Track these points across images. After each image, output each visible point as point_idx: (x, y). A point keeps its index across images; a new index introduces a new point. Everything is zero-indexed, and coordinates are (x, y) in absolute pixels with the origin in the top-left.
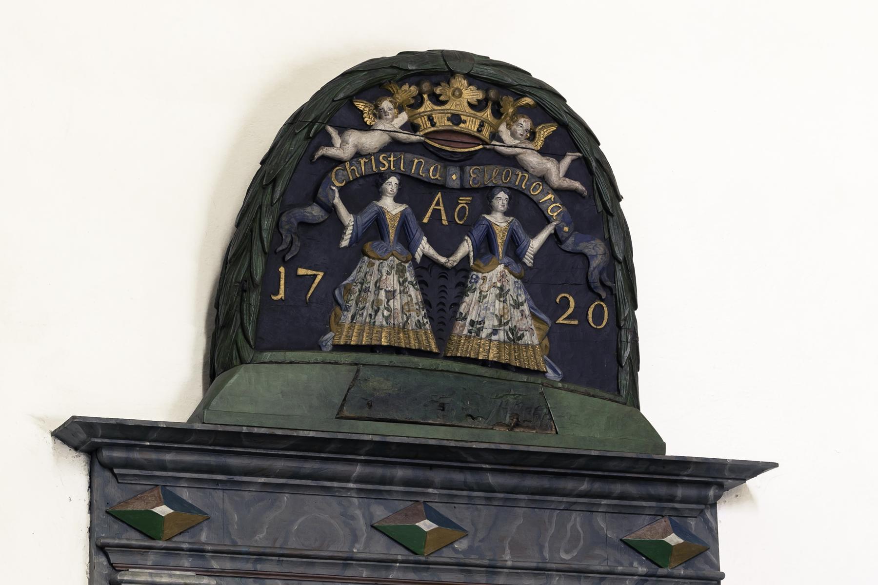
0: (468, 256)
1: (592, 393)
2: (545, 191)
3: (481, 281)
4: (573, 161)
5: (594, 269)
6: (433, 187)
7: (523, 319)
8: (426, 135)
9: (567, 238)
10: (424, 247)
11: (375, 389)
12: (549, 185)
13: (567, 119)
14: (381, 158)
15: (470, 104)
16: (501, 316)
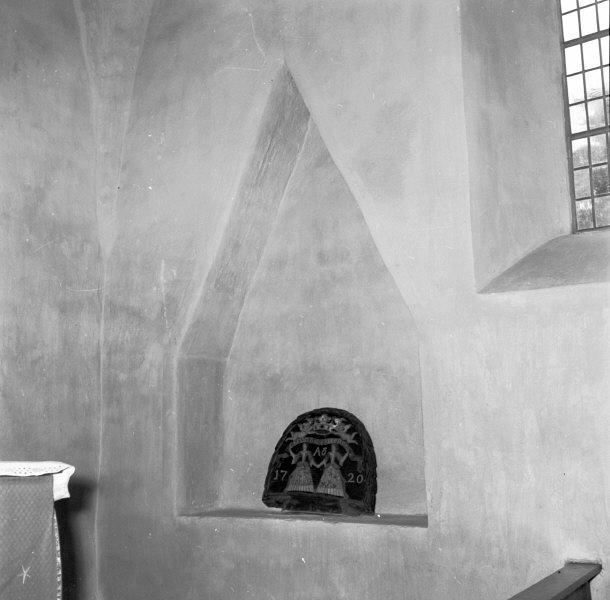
10: (313, 463)
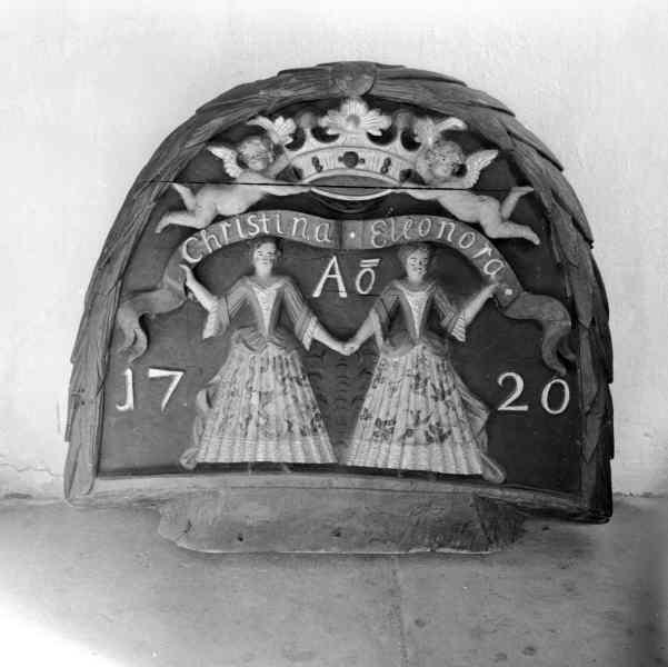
10: (312, 332)
15: (373, 138)
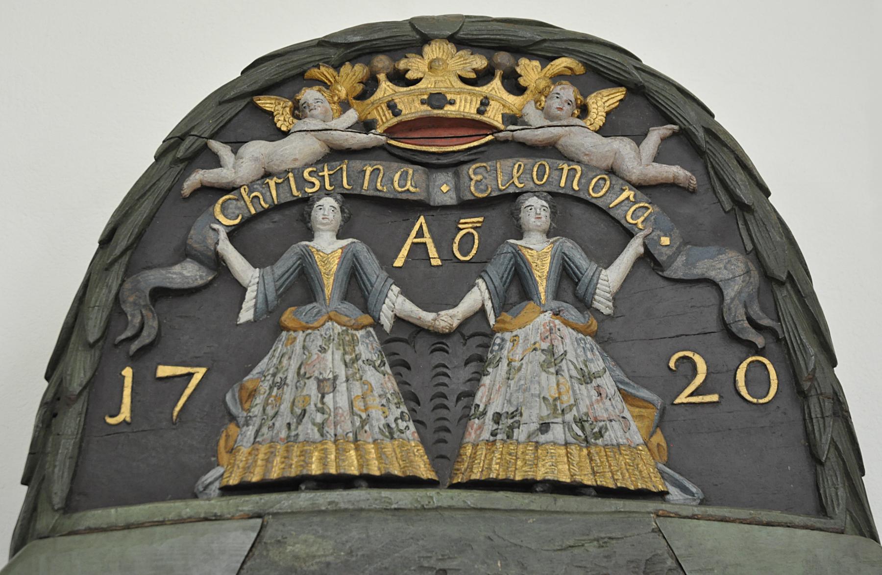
0: (482, 311)
1: (765, 519)
2: (617, 188)
3: (508, 345)
4: (664, 140)
5: (733, 299)
6: (407, 207)
7: (603, 399)
8: (390, 132)
9: (672, 258)
10: (395, 303)
11: (296, 557)
12: (623, 179)
13: (639, 77)
14: (306, 174)
16: (555, 400)
